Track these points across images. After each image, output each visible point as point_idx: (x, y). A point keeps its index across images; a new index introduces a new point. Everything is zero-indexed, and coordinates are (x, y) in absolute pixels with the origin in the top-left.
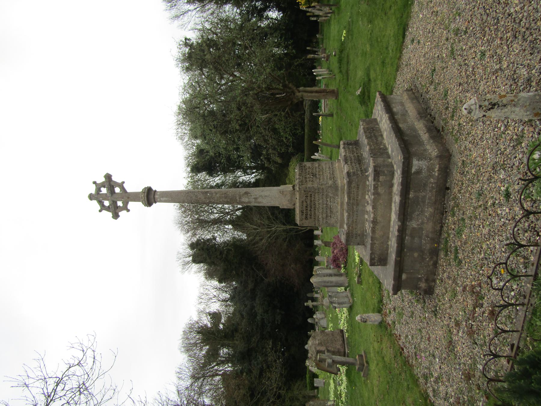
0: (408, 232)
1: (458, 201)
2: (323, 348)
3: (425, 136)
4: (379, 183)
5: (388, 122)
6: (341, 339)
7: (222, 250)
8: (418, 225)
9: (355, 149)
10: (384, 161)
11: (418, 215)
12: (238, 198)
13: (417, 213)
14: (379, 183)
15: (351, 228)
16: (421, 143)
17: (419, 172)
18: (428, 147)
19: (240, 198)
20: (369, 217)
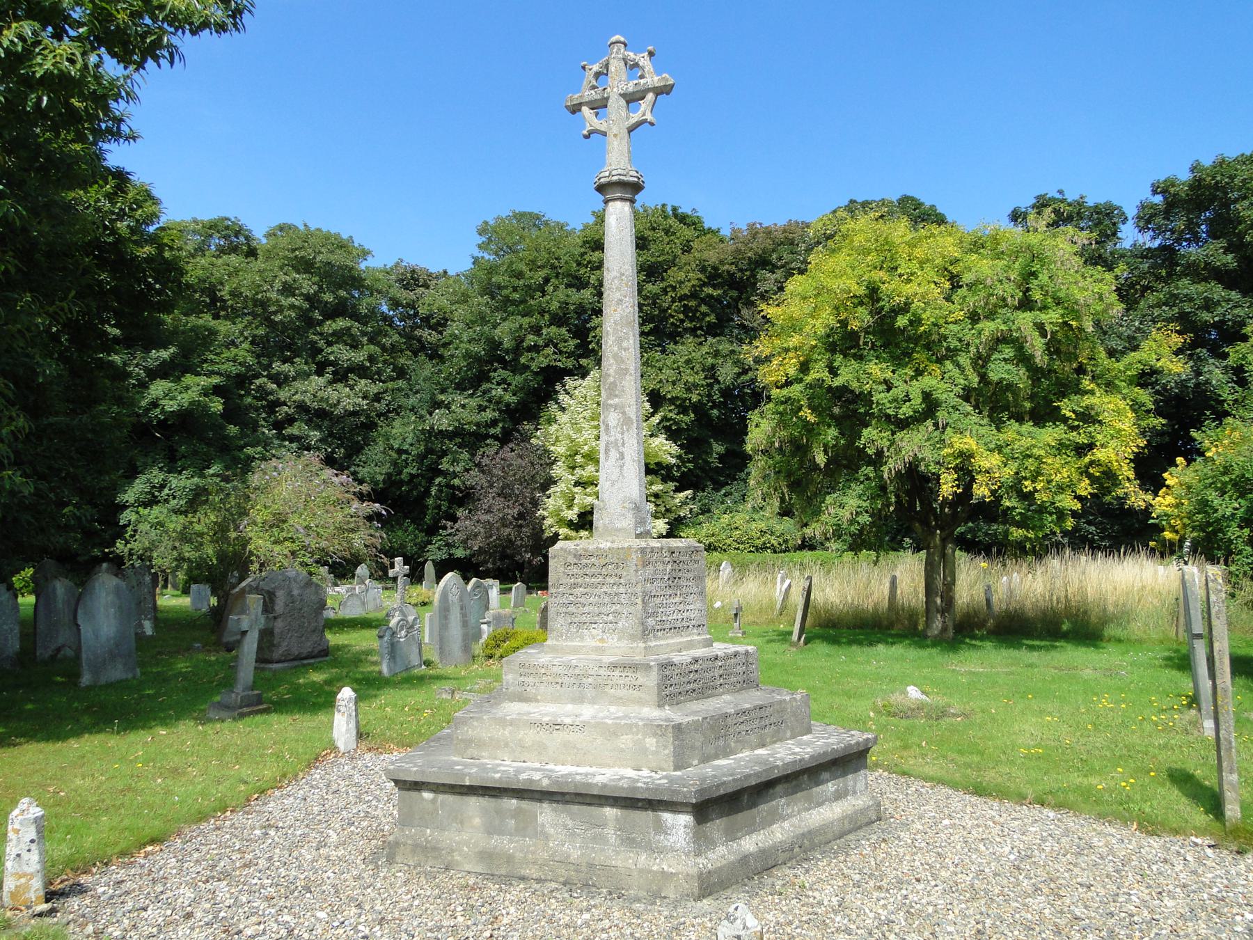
0: (525, 804)
1: (94, 870)
2: (279, 606)
3: (749, 844)
4: (640, 736)
5: (790, 758)
6: (305, 652)
7: (540, 378)
8: (543, 825)
9: (733, 679)
10: (693, 748)
11: (565, 826)
12: (616, 400)
13: (570, 823)
14: (640, 736)
15: (543, 671)
16: (732, 835)
17: (660, 828)
18: (721, 850)
19: (616, 407)
20: (565, 711)
